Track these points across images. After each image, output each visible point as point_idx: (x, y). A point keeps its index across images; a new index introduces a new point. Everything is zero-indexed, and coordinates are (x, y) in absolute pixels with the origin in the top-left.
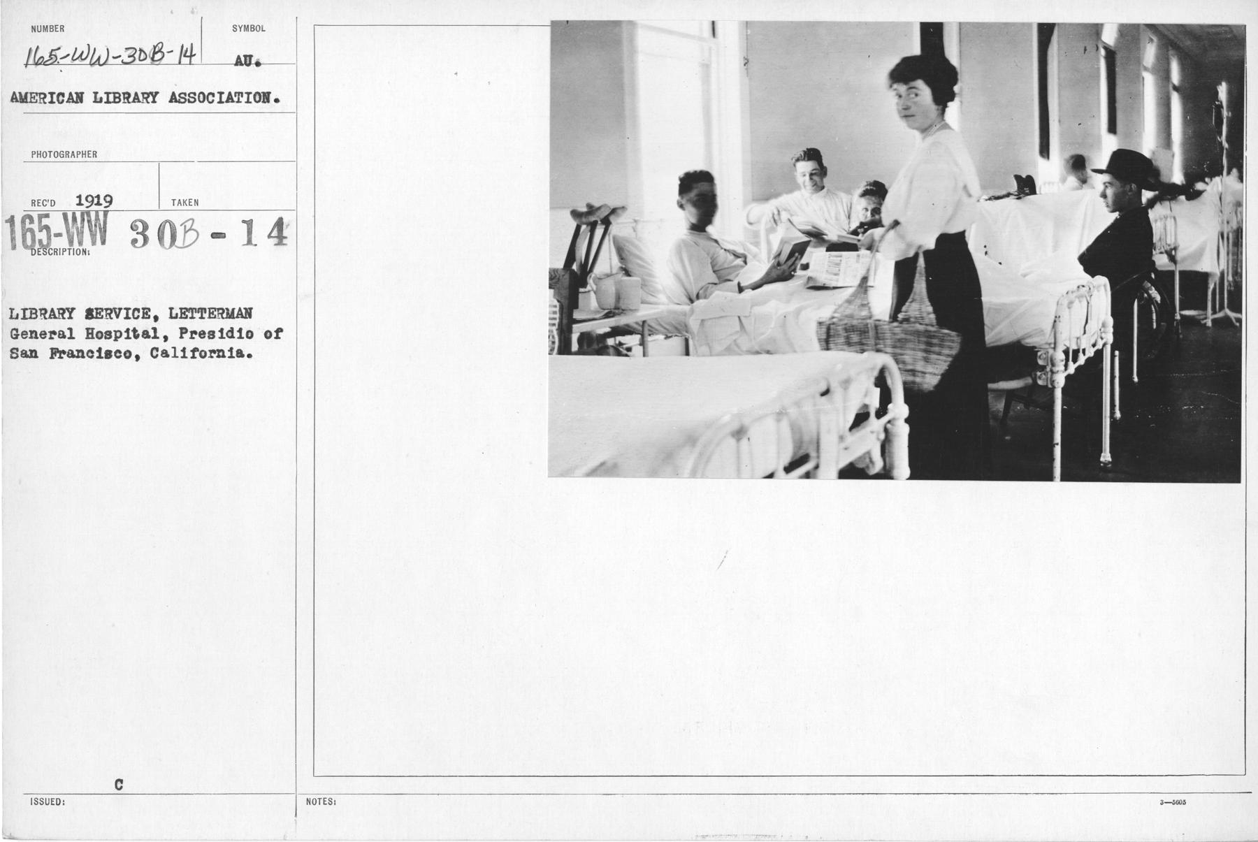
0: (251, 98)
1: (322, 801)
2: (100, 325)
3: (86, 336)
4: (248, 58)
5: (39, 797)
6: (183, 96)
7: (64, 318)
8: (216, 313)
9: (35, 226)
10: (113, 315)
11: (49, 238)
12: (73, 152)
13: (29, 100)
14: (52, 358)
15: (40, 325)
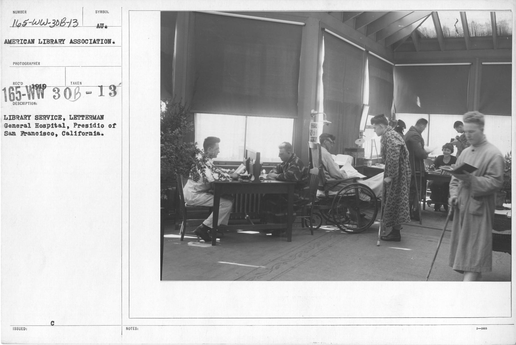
0: (103, 42)
1: (132, 328)
2: (41, 122)
3: (35, 127)
4: (102, 25)
5: (16, 327)
6: (75, 40)
7: (26, 119)
8: (89, 117)
9: (14, 92)
10: (47, 118)
11: (20, 96)
12: (30, 63)
13: (12, 43)
14: (21, 135)
15: (16, 122)
